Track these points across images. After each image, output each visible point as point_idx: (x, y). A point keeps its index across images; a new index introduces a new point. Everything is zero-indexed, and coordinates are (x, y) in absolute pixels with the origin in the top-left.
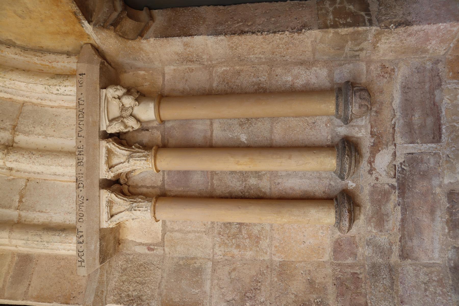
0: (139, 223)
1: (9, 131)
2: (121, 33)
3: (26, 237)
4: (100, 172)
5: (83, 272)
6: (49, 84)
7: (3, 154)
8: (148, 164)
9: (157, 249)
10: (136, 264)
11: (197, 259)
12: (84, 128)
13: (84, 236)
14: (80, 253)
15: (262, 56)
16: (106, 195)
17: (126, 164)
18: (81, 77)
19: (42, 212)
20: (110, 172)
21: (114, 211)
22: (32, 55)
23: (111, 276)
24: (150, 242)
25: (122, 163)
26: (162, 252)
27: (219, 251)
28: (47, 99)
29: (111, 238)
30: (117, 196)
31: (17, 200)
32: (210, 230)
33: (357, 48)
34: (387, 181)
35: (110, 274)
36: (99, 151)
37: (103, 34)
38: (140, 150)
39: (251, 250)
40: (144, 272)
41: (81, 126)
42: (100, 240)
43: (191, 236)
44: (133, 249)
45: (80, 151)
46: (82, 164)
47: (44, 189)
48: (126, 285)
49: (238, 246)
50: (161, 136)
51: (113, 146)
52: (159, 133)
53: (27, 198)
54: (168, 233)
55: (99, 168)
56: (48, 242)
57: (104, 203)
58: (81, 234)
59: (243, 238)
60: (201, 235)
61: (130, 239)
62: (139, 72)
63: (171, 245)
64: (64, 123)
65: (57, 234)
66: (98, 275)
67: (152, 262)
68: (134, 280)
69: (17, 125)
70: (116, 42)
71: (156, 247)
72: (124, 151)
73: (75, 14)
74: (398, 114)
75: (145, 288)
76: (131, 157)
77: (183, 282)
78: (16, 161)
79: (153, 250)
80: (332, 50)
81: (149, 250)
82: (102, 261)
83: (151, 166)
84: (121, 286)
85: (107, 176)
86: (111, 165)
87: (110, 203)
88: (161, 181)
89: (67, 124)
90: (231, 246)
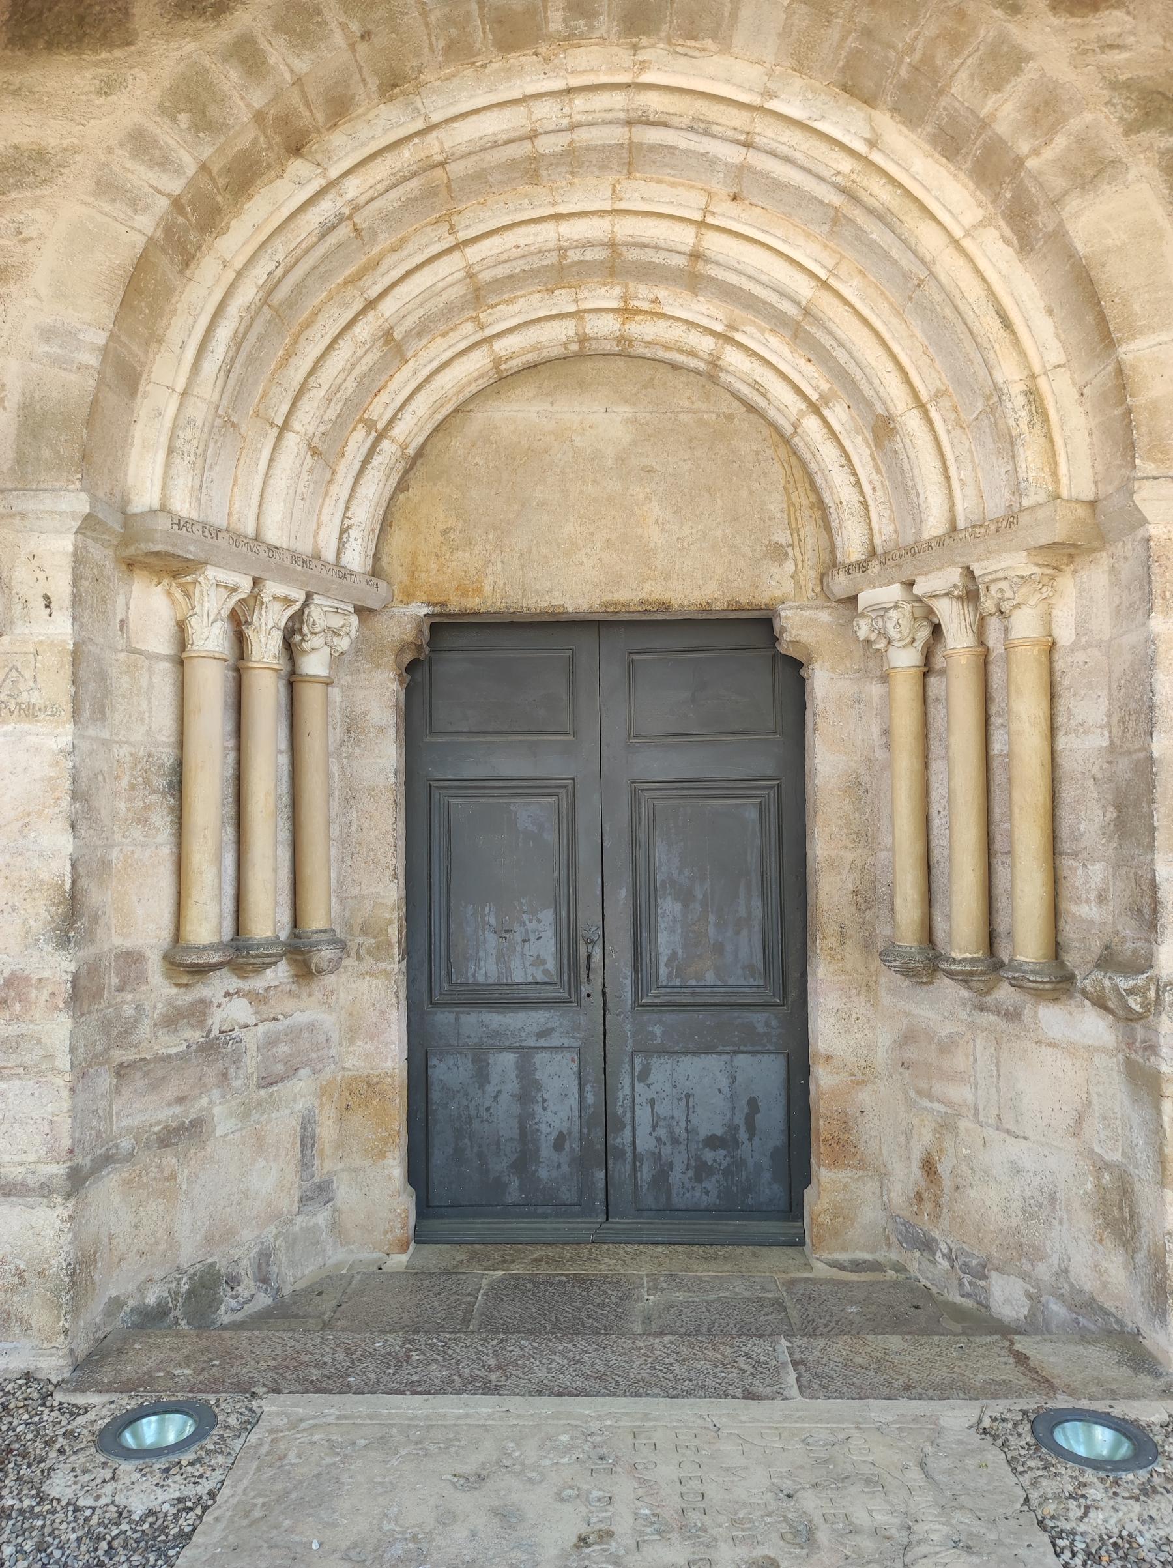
15: (354, 828)
26: (120, 648)
27: (123, 752)
33: (363, 952)
34: (217, 1020)
39: (129, 810)
49: (133, 787)
59: (145, 797)
73: (444, 604)
74: (287, 1022)
80: (359, 921)
90: (132, 775)
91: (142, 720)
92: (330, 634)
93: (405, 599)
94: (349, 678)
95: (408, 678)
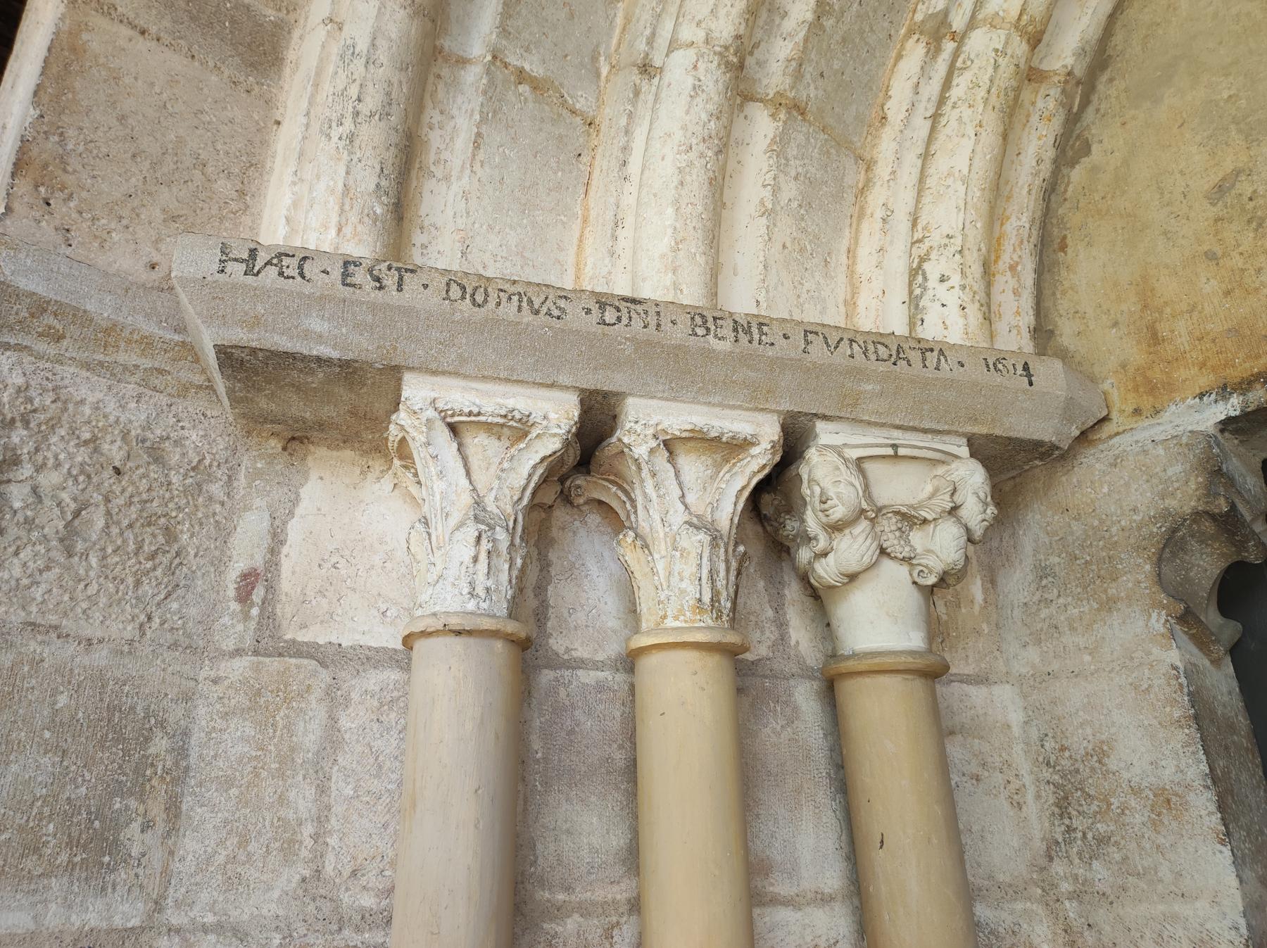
0: (393, 546)
1: (792, 88)
2: (1183, 538)
3: (382, 56)
4: (654, 402)
5: (191, 259)
6: (966, 252)
7: (726, 48)
8: (681, 611)
9: (246, 617)
10: (179, 508)
11: (168, 835)
12: (840, 357)
13: (380, 294)
14: (294, 262)
16: (556, 416)
17: (678, 516)
18: (1020, 371)
19: (477, 146)
20: (653, 444)
21: (478, 443)
22: (1034, 212)
23: (131, 389)
24: (287, 583)
26: (229, 645)
28: (888, 238)
29: (328, 412)
30: (543, 460)
31: (527, 67)
32: (327, 907)
35: (144, 383)
36: (740, 407)
37: (1178, 468)
40: (132, 547)
42: (344, 364)
43: (302, 799)
44: (258, 502)
45: (748, 331)
46: (701, 331)
47: (555, 173)
48: (71, 456)
51: (755, 466)
53: (531, 105)
54: (325, 676)
55: (674, 399)
56: (351, 138)
57: (520, 400)
58: (390, 281)
60: (304, 853)
61: (305, 492)
62: (979, 582)
63: (258, 693)
64: (807, 285)
65: (384, 183)
66: (149, 328)
67: (180, 592)
68: (97, 498)
69: (804, 120)
70: (1135, 510)
71: (255, 611)
72: (730, 509)
75: (41, 549)
76: (714, 539)
77: (45, 761)
78: (697, 88)
79: (244, 596)
81: (245, 576)
82: (232, 359)
83: (670, 623)
84: (72, 432)
85: (638, 428)
86: (679, 448)
87: (516, 429)
88: (568, 650)
89: (804, 296)
91: (289, 849)
92: (889, 525)
93: (1147, 403)
94: (1033, 654)
95: (1230, 630)
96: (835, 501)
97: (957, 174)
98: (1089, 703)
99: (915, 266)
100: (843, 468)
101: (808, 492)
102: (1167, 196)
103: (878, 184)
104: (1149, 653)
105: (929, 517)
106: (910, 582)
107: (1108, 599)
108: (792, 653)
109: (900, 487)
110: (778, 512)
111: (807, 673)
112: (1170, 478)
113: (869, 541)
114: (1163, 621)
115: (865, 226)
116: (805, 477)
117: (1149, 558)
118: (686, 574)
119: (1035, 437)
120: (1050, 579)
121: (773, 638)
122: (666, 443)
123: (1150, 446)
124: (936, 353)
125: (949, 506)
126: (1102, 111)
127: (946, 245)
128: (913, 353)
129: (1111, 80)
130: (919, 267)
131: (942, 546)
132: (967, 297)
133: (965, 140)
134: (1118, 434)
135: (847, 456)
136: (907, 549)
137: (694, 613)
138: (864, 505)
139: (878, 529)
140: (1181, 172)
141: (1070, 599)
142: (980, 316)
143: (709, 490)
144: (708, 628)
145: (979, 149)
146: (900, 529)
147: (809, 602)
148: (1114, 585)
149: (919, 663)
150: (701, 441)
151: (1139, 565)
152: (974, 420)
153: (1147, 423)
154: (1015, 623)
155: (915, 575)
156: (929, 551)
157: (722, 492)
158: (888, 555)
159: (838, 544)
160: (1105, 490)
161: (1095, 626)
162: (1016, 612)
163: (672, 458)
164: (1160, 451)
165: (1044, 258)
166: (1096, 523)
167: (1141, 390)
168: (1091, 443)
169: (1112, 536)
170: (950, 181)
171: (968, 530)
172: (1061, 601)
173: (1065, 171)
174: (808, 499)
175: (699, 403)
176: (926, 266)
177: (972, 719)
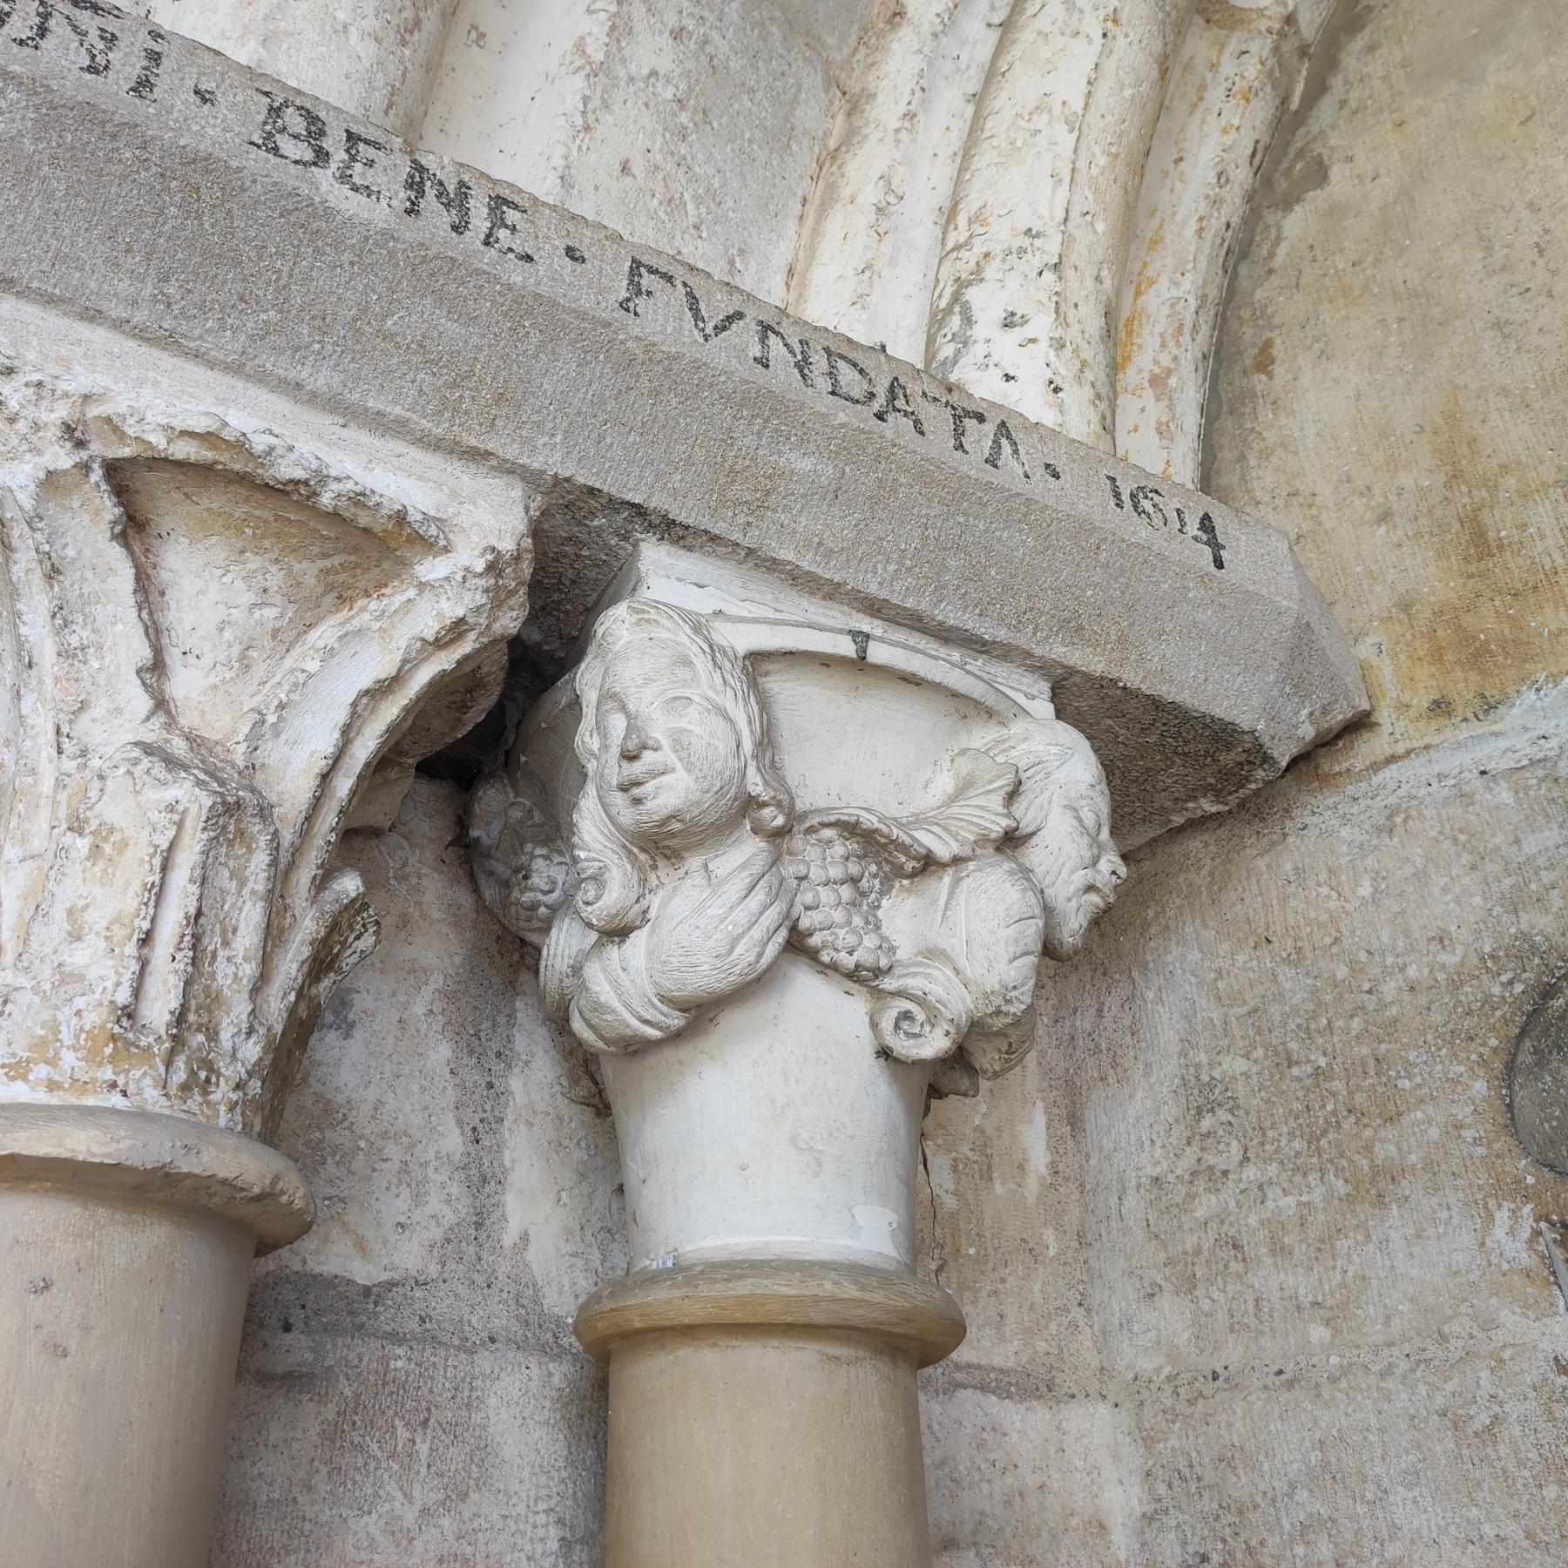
4: (98, 336)
6: (1069, 272)
18: (1193, 528)
20: (63, 458)
25: (157, 667)
38: (291, 964)
41: (745, 334)
50: (363, 1272)
51: (429, 619)
52: (409, 1256)
55: (169, 342)
62: (1040, 1119)
70: (1441, 939)
72: (324, 742)
86: (171, 510)
92: (824, 860)
93: (1463, 686)
94: (1171, 1318)
96: (666, 755)
97: (1057, 109)
98: (1326, 1465)
99: (943, 304)
100: (702, 663)
101: (595, 744)
102: (1500, 254)
103: (874, 137)
104: (1489, 1324)
105: (943, 852)
106: (868, 1046)
107: (1376, 1172)
108: (503, 1268)
109: (862, 759)
110: (518, 837)
111: (535, 1335)
112: (1530, 859)
113: (759, 896)
114: (1525, 1234)
115: (835, 223)
116: (590, 698)
117: (1483, 1062)
118: (97, 918)
119: (1219, 712)
120: (1223, 1115)
121: (450, 1217)
122: (113, 469)
123: (1478, 783)
124: (989, 428)
125: (997, 826)
126: (1353, 104)
127: (1022, 251)
128: (932, 408)
129: (1372, 48)
130: (956, 297)
131: (970, 943)
132: (1065, 371)
133: (1078, 45)
134: (1393, 759)
135: (717, 639)
136: (870, 941)
137: (92, 1056)
138: (755, 784)
139: (790, 869)
140: (1532, 207)
141: (1273, 1168)
142: (1095, 418)
143: (259, 671)
144: (142, 1116)
145: (1109, 66)
146: (854, 881)
147: (577, 1118)
148: (1390, 1132)
149: (878, 1303)
150: (229, 478)
151: (1456, 1082)
152: (1073, 629)
153: (1465, 732)
154: (1125, 1231)
155: (887, 1024)
156: (933, 954)
157: (304, 683)
158: (812, 955)
159: (665, 904)
160: (1365, 890)
161: (1342, 1244)
162: (1131, 1201)
163: (134, 528)
164: (1504, 795)
165: (1222, 386)
166: (1342, 972)
167: (1450, 657)
168: (1327, 781)
169: (1383, 1006)
170: (1041, 121)
171: (1048, 910)
172: (1251, 1173)
173: (1270, 217)
174: (591, 767)
175: (261, 378)
176: (972, 295)
177: (1008, 1503)
